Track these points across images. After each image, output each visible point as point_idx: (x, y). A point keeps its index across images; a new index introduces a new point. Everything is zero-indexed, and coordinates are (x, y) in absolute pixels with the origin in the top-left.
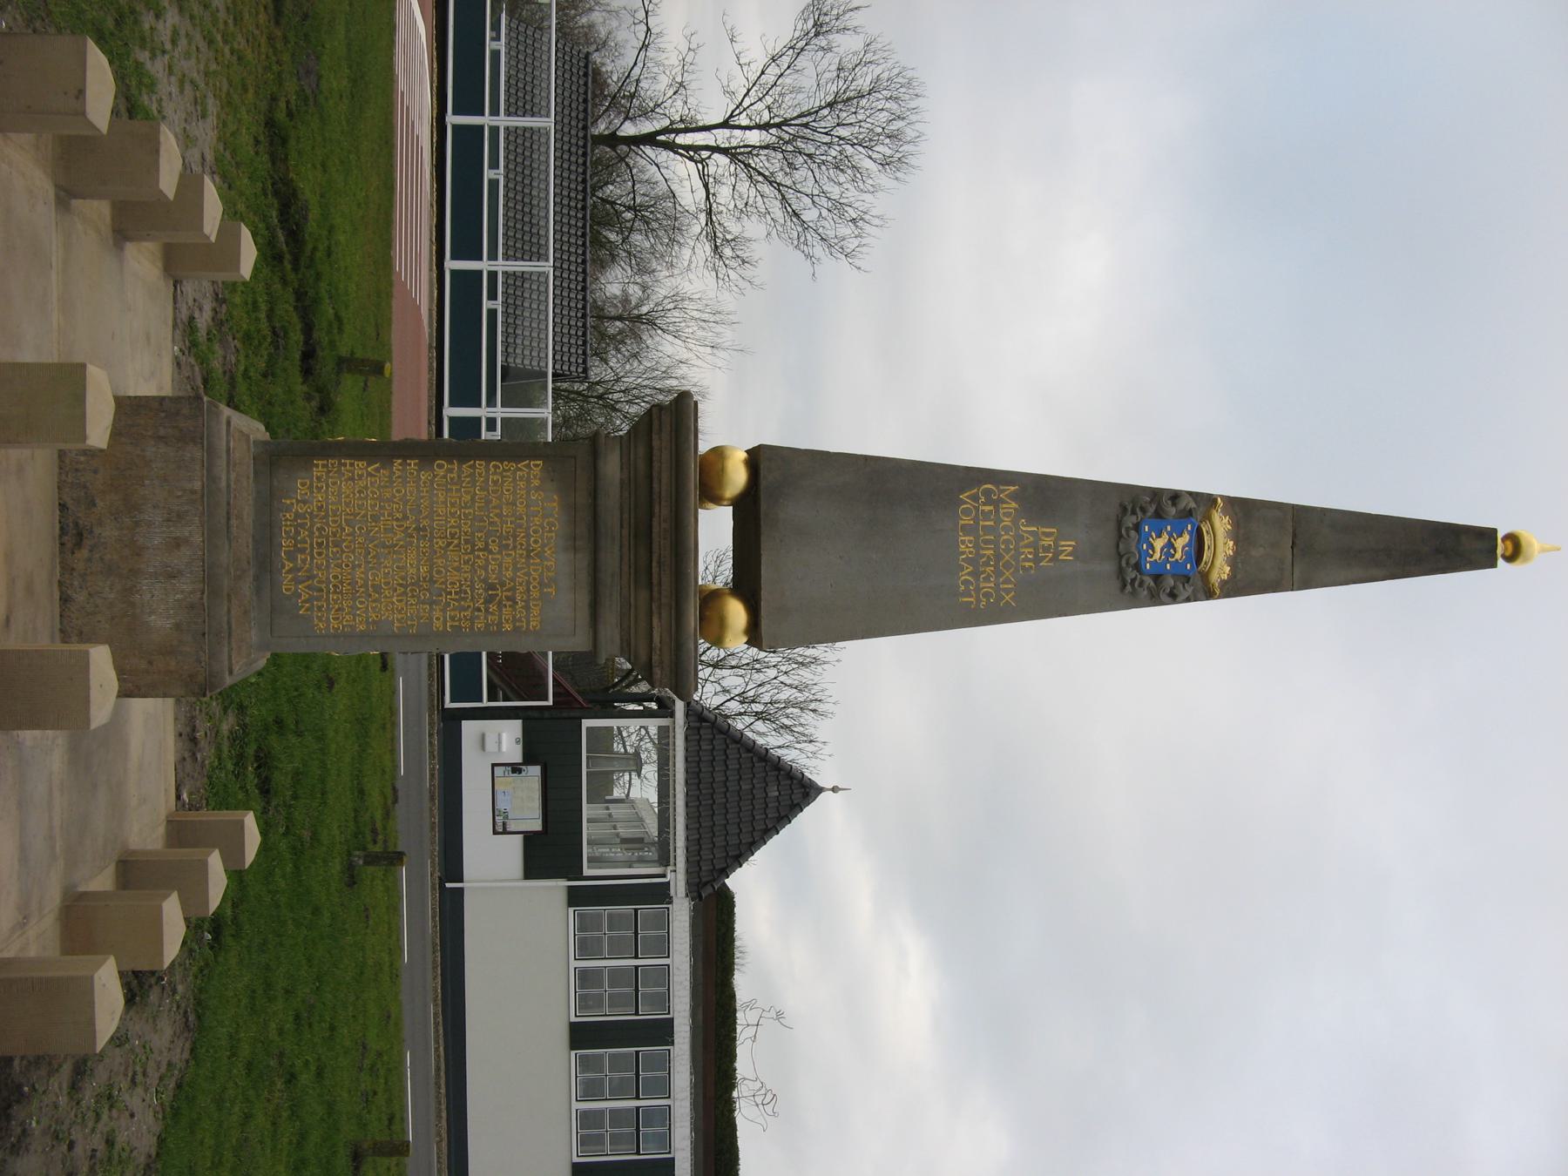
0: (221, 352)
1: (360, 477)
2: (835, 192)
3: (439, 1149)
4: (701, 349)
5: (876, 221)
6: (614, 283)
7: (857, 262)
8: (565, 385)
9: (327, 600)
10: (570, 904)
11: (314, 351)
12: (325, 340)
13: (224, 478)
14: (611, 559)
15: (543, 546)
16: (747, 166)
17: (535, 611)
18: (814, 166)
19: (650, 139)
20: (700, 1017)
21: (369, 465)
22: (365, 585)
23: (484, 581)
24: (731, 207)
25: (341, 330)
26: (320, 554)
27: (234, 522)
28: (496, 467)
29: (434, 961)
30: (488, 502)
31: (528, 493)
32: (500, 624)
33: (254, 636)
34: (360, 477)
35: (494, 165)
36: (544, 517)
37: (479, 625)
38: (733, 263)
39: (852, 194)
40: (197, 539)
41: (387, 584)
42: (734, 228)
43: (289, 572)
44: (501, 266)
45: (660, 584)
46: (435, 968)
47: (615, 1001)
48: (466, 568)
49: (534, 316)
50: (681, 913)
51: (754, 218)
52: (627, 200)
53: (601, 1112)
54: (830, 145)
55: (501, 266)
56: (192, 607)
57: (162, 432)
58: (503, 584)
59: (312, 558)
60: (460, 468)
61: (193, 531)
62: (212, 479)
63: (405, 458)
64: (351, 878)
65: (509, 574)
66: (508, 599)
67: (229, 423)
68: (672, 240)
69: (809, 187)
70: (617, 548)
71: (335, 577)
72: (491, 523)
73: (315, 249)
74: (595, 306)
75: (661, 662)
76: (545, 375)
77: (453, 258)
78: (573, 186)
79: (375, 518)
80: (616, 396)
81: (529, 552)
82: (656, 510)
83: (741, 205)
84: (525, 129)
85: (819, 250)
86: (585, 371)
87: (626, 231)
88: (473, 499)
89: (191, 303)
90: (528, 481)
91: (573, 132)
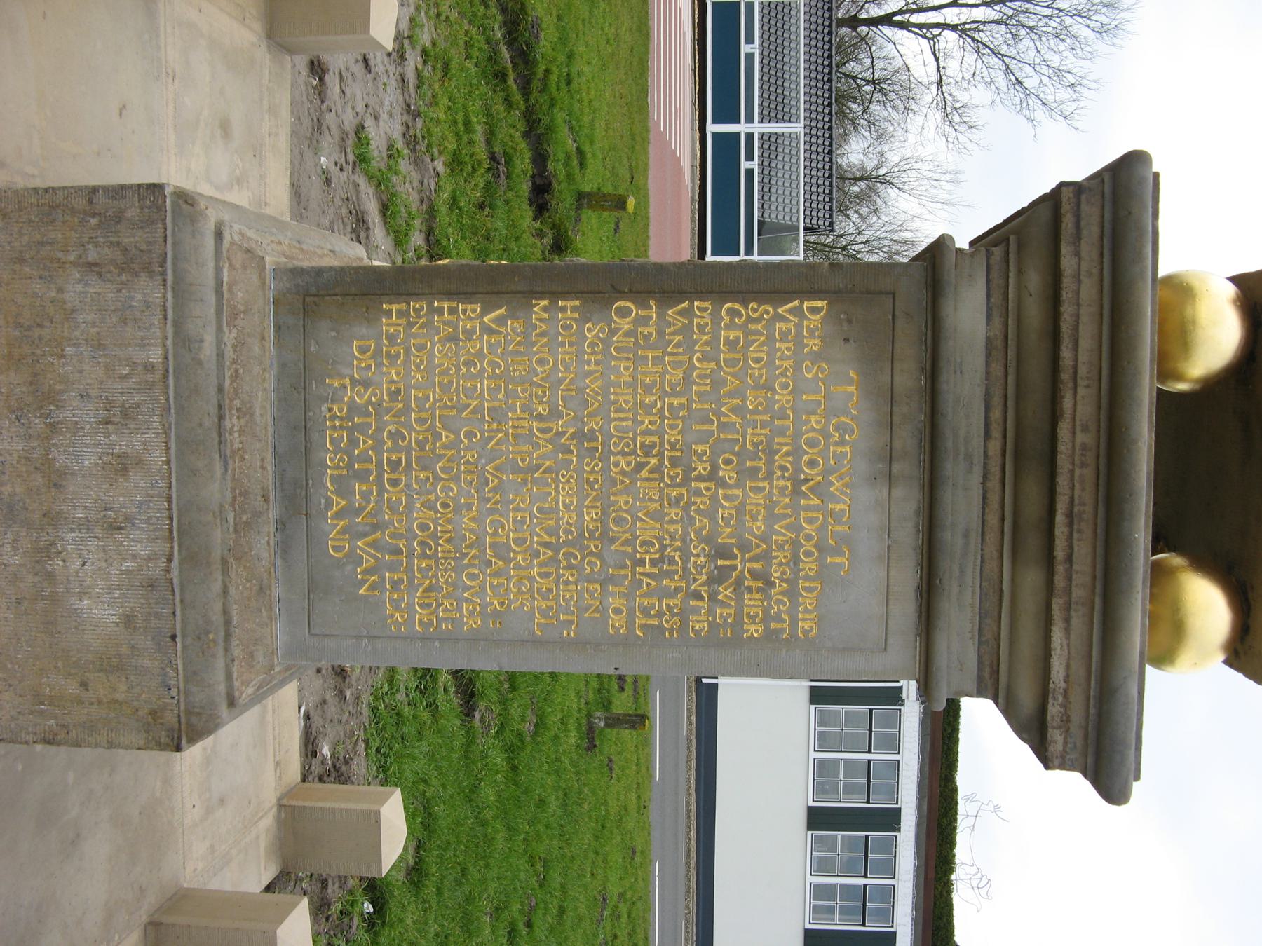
0: (415, 176)
1: (469, 334)
2: (1055, 60)
3: (687, 920)
4: (934, 205)
5: (1093, 86)
6: (855, 152)
7: (1076, 124)
8: (812, 239)
9: (409, 569)
10: (812, 702)
11: (550, 184)
12: (562, 175)
13: (209, 339)
14: (965, 502)
15: (826, 472)
16: (973, 39)
17: (808, 601)
18: (1036, 37)
19: (887, 20)
20: (925, 807)
21: (485, 312)
22: (478, 543)
23: (709, 540)
24: (959, 79)
25: (582, 164)
26: (394, 483)
27: (232, 422)
28: (733, 313)
29: (689, 756)
30: (717, 384)
31: (798, 367)
32: (738, 621)
33: (279, 633)
34: (469, 334)
35: (750, 40)
36: (830, 413)
37: (698, 624)
38: (963, 128)
39: (1070, 62)
40: (157, 457)
41: (520, 542)
42: (963, 97)
43: (339, 515)
44: (757, 128)
45: (1069, 559)
46: (688, 761)
47: (849, 789)
48: (673, 512)
49: (787, 176)
50: (911, 714)
51: (981, 86)
52: (868, 75)
53: (832, 887)
54: (1050, 17)
55: (757, 128)
56: (151, 585)
57: (92, 255)
58: (744, 547)
59: (381, 490)
60: (661, 316)
61: (148, 442)
62: (185, 341)
63: (554, 296)
64: (590, 739)
65: (758, 526)
66: (755, 575)
67: (219, 235)
68: (907, 109)
69: (1031, 56)
70: (976, 477)
71: (423, 527)
72: (723, 427)
73: (547, 71)
74: (840, 167)
75: (1066, 719)
76: (797, 229)
77: (714, 122)
78: (820, 61)
79: (498, 415)
80: (857, 247)
81: (797, 483)
82: (1067, 403)
83: (968, 76)
84: (770, 135)
85: (1040, 113)
86: (831, 224)
87: (867, 103)
88: (687, 378)
89: (360, 108)
90: (799, 343)
91: (820, 13)
